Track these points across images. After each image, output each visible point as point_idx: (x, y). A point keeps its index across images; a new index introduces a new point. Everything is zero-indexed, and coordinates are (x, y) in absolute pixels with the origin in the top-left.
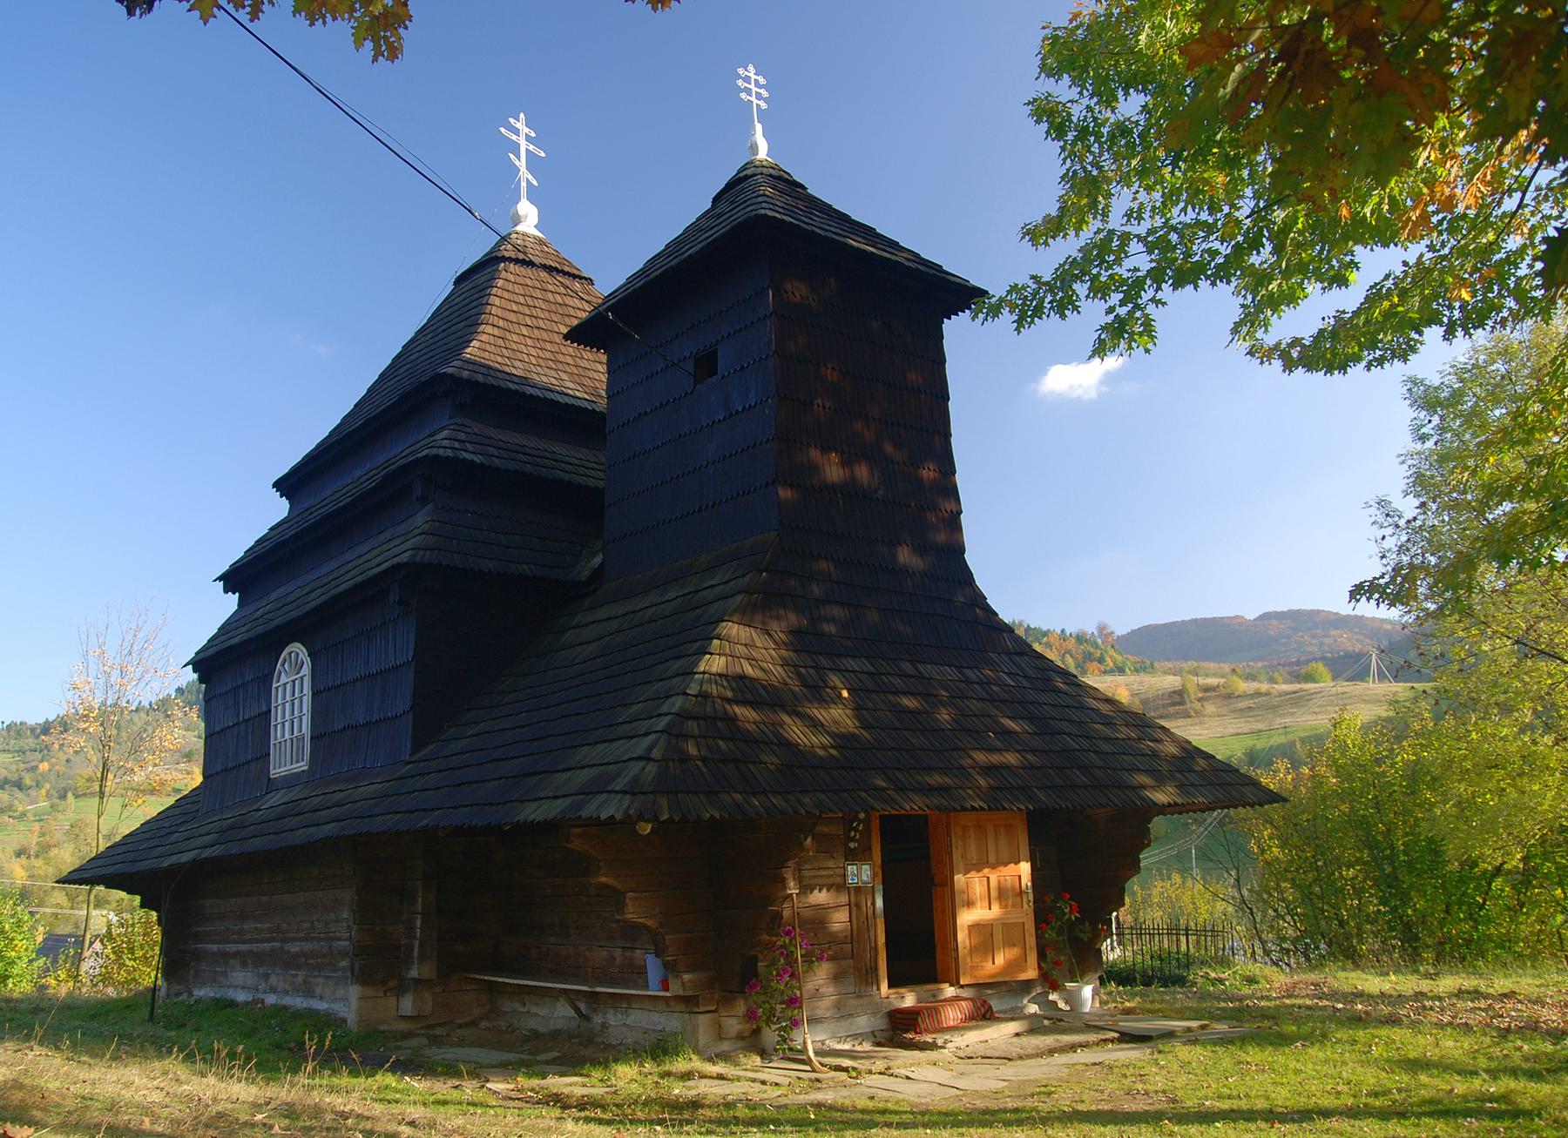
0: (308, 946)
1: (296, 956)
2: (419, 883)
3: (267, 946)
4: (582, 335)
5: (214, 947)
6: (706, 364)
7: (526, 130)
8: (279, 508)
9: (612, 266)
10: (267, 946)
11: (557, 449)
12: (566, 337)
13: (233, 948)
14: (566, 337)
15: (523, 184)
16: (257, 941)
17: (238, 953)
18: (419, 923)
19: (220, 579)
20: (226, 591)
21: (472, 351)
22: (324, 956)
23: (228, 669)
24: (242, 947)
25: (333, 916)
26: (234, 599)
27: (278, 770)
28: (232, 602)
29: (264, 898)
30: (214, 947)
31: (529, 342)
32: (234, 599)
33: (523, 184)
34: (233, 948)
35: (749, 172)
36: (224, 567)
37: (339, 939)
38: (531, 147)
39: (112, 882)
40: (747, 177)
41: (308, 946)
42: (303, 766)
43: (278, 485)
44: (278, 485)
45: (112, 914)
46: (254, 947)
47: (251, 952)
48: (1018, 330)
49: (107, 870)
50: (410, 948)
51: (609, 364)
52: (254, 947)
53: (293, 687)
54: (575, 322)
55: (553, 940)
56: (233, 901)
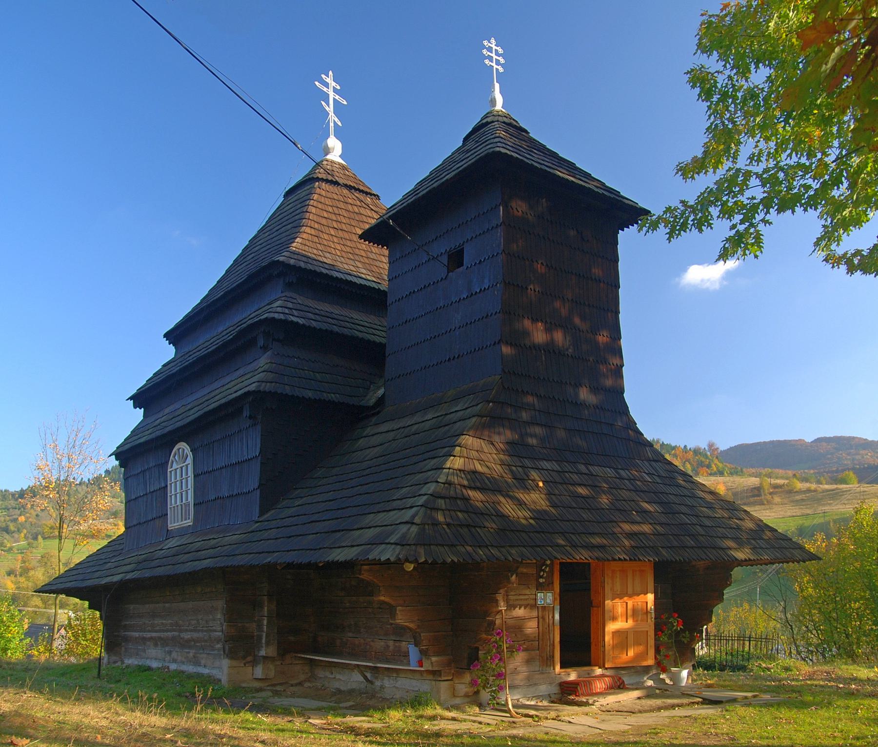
1: (188, 641)
2: (265, 598)
3: (170, 634)
5: (136, 634)
6: (456, 259)
7: (334, 84)
8: (169, 352)
13: (148, 635)
14: (361, 237)
15: (332, 124)
16: (163, 631)
17: (151, 638)
18: (265, 622)
19: (131, 398)
20: (135, 407)
22: (206, 641)
25: (211, 617)
26: (140, 412)
28: (139, 414)
29: (167, 605)
30: (136, 634)
31: (335, 240)
32: (140, 412)
33: (332, 124)
34: (148, 635)
35: (489, 119)
37: (216, 631)
38: (337, 97)
40: (488, 123)
42: (189, 522)
43: (167, 336)
44: (167, 336)
45: (70, 612)
46: (162, 635)
47: (160, 638)
51: (390, 257)
52: (162, 635)
55: (350, 634)
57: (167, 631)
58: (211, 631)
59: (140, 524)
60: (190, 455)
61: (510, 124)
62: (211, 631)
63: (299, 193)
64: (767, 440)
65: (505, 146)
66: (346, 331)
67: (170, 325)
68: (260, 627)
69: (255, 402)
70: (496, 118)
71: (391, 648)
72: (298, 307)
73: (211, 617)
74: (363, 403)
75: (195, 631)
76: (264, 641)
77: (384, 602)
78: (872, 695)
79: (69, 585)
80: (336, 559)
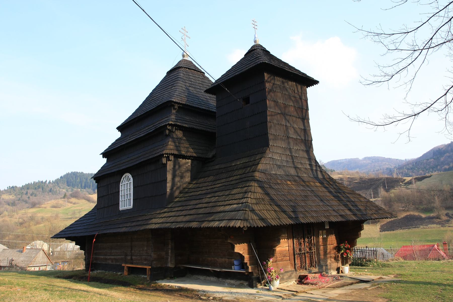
5: (102, 257)
6: (247, 100)
8: (118, 135)
11: (171, 284)
13: (108, 257)
16: (116, 255)
17: (110, 259)
18: (170, 252)
19: (101, 154)
20: (103, 157)
23: (105, 181)
24: (113, 257)
26: (105, 160)
27: (122, 207)
28: (105, 160)
29: (119, 244)
30: (102, 257)
32: (105, 160)
34: (108, 257)
35: (256, 48)
36: (103, 151)
39: (71, 239)
40: (255, 49)
46: (115, 257)
47: (115, 259)
48: (316, 82)
49: (67, 234)
50: (167, 259)
51: (217, 98)
52: (115, 257)
53: (127, 187)
56: (108, 244)
57: (119, 255)
59: (105, 207)
60: (132, 179)
61: (263, 50)
64: (230, 68)
67: (119, 124)
68: (167, 254)
70: (258, 48)
71: (227, 262)
72: (180, 119)
74: (207, 157)
76: (169, 260)
77: (229, 243)
79: (70, 235)
80: (214, 226)
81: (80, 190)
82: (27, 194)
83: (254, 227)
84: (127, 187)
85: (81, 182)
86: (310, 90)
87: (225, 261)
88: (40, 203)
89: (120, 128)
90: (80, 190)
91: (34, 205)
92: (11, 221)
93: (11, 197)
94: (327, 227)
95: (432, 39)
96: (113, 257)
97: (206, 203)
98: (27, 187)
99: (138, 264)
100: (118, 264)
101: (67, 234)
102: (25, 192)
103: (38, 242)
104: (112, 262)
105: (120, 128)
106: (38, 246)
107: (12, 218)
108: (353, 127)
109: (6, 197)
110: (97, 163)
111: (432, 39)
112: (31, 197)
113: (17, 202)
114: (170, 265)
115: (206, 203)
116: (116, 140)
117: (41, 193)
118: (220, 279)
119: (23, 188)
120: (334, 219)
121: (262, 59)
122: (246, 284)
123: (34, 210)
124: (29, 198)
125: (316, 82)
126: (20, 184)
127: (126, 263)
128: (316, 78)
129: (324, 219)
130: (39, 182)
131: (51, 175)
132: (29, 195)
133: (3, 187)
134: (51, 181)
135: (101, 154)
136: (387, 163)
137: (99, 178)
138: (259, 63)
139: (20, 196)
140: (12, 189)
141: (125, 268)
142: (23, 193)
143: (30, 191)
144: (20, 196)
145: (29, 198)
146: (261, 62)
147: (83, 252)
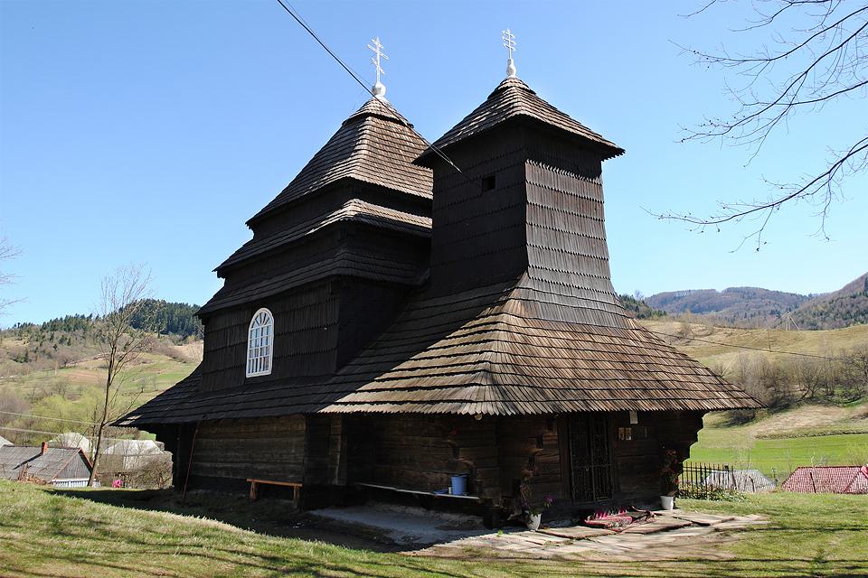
0: (268, 467)
1: (263, 471)
2: (339, 437)
3: (243, 465)
4: (423, 161)
6: (490, 182)
7: (380, 45)
9: (434, 127)
10: (243, 465)
12: (414, 163)
14: (414, 163)
15: (378, 74)
17: (224, 468)
18: (339, 457)
19: (215, 270)
20: (697, 441)
21: (431, 197)
22: (279, 472)
23: (221, 322)
24: (229, 465)
25: (285, 451)
28: (221, 283)
29: (241, 440)
31: (386, 159)
32: (221, 283)
33: (378, 74)
37: (289, 463)
38: (382, 55)
40: (508, 88)
41: (268, 467)
42: (268, 372)
43: (248, 223)
44: (248, 223)
45: (149, 445)
48: (620, 152)
49: (147, 419)
53: (262, 331)
54: (417, 156)
55: (406, 467)
58: (286, 463)
62: (286, 463)
63: (355, 124)
65: (523, 108)
66: (376, 214)
69: (339, 283)
73: (285, 451)
75: (267, 463)
77: (449, 443)
78: (827, 388)
81: (157, 335)
82: (52, 338)
83: (495, 414)
84: (262, 331)
85: (160, 317)
86: (606, 165)
87: (442, 479)
88: (76, 360)
89: (252, 224)
90: (157, 335)
91: (64, 363)
92: (18, 391)
93: (20, 343)
94: (634, 421)
95: (806, 72)
96: (229, 465)
97: (409, 370)
98: (53, 326)
99: (276, 480)
100: (239, 477)
101: (147, 419)
102: (48, 336)
103: (72, 435)
104: (228, 474)
105: (252, 224)
106: (70, 442)
107: (21, 385)
108: (688, 232)
109: (11, 343)
110: (202, 288)
111: (806, 72)
112: (59, 346)
113: (31, 355)
114: (336, 482)
115: (409, 370)
116: (729, 290)
117: (79, 338)
118: (432, 513)
119: (44, 327)
120: (645, 406)
121: (519, 108)
122: (479, 521)
123: (64, 373)
124: (55, 347)
125: (620, 152)
126: (39, 320)
127: (255, 476)
128: (618, 145)
129: (625, 406)
130: (77, 316)
131: (94, 303)
132: (56, 341)
133: (8, 323)
134: (101, 316)
135: (215, 270)
136: (773, 301)
137: (208, 315)
138: (514, 114)
139: (38, 343)
140: (23, 329)
141: (253, 486)
142: (44, 337)
143: (58, 335)
144: (38, 343)
145: (55, 347)
146: (518, 113)
147: (169, 454)
